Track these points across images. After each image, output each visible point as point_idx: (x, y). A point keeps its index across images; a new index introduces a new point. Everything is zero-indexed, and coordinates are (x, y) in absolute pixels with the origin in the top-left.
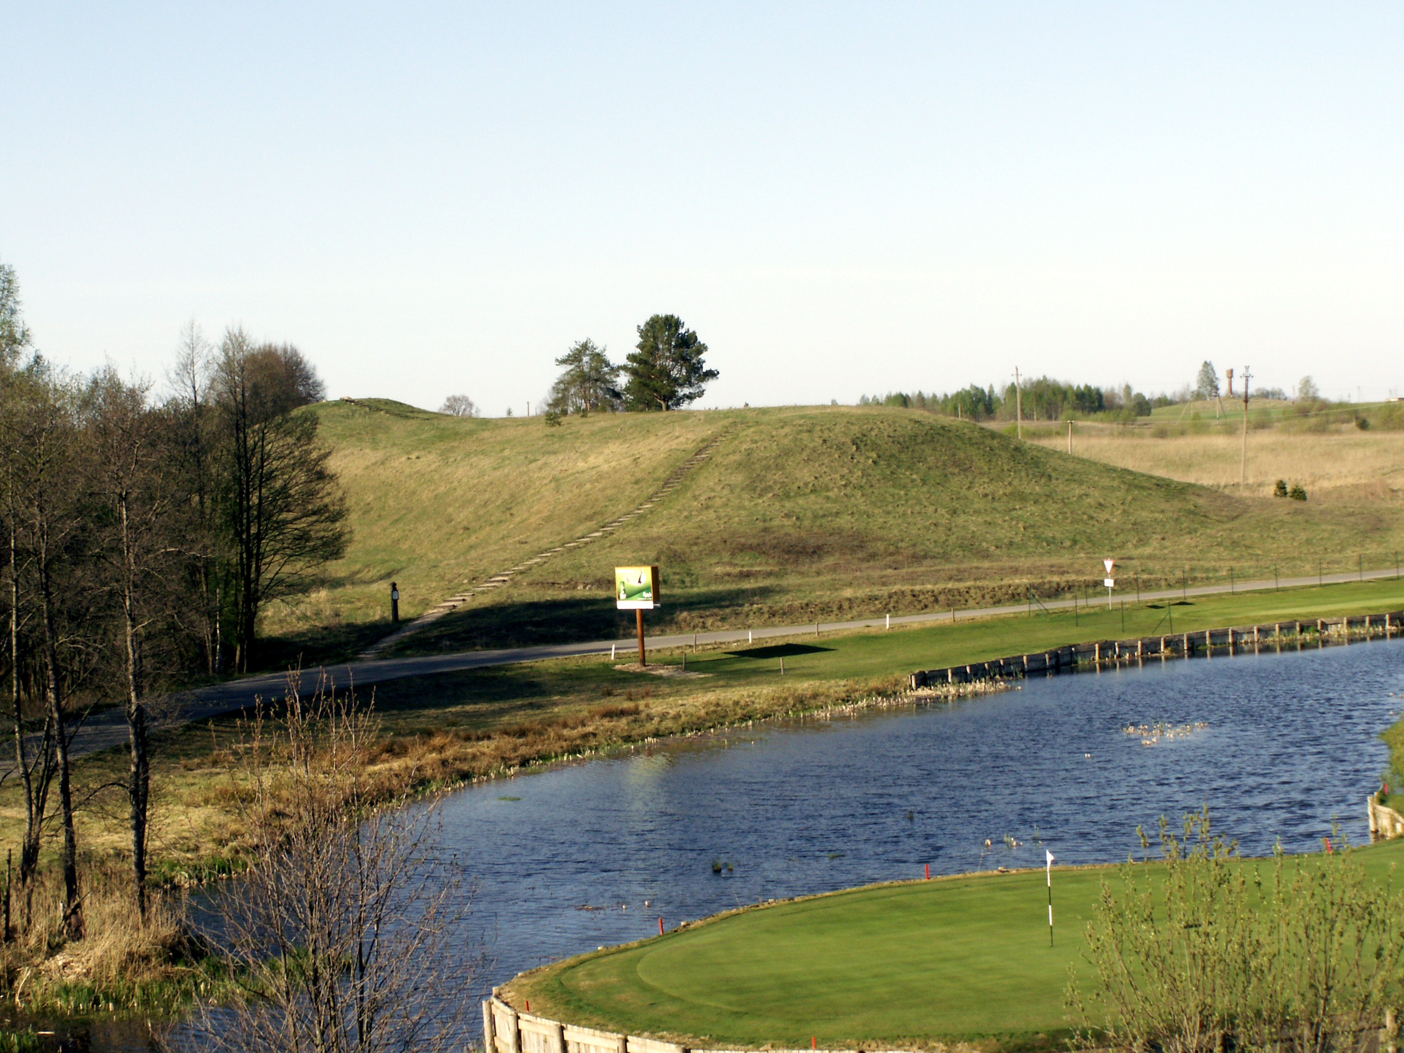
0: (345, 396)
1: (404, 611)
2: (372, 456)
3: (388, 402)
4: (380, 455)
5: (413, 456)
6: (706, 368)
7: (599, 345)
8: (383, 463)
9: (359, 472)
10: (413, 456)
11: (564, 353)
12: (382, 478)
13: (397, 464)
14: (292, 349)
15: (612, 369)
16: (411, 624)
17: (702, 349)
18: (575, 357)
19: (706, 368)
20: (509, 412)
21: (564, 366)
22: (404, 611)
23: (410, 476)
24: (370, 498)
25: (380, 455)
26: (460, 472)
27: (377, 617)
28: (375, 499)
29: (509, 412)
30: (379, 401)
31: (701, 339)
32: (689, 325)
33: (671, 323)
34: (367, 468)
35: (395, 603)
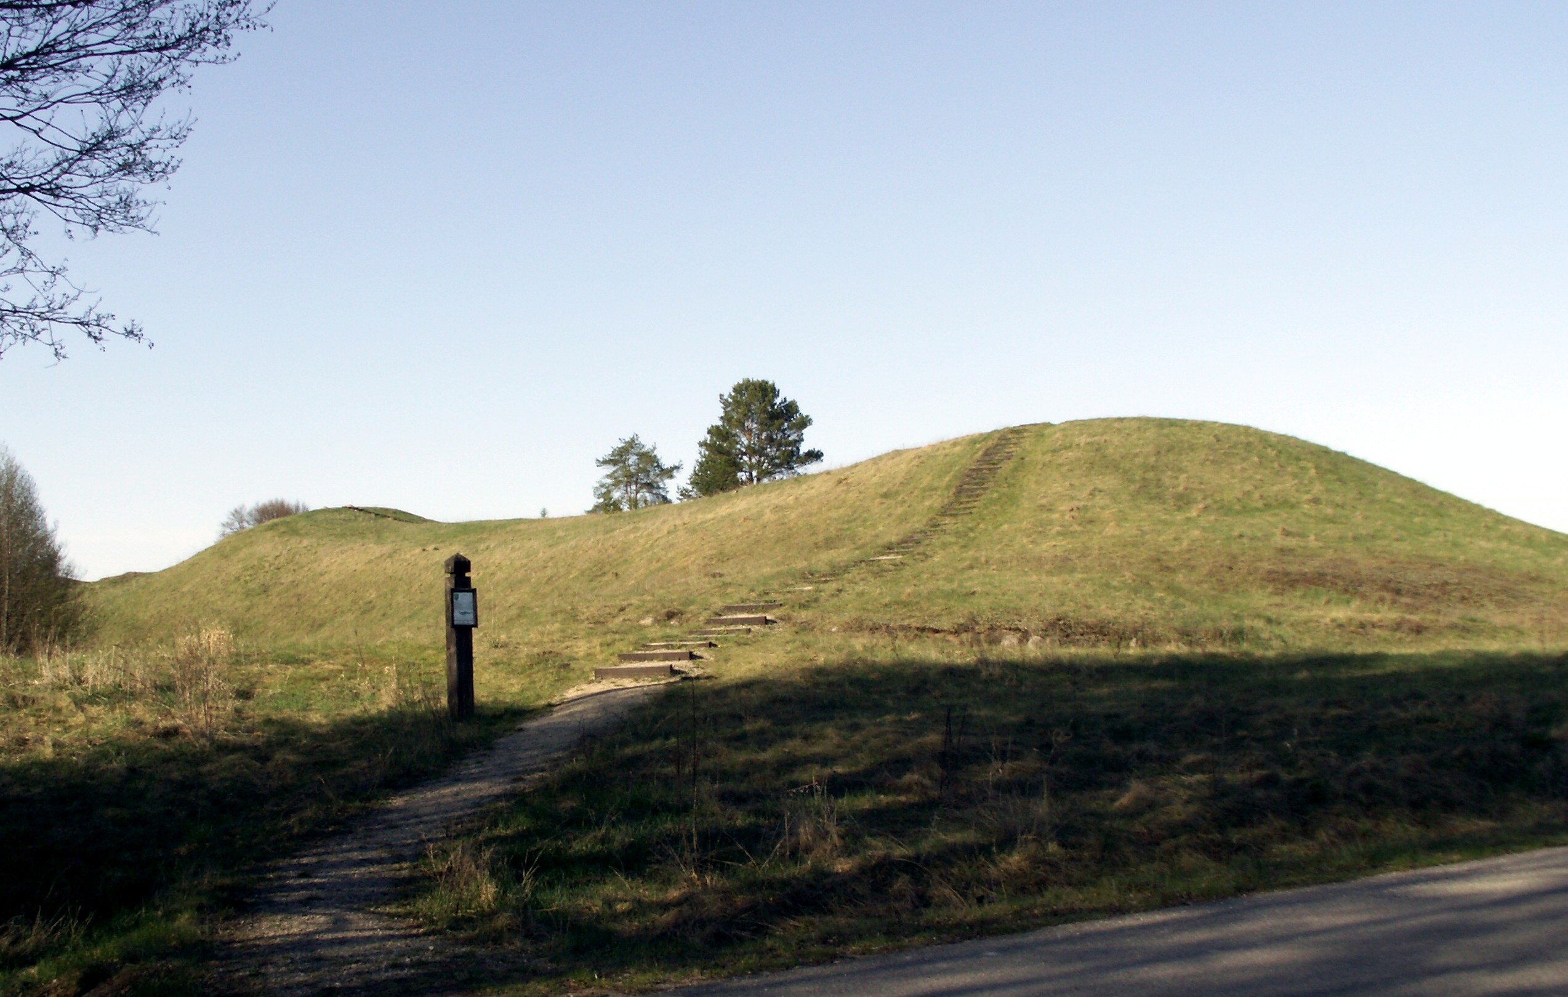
0: (348, 504)
1: (491, 684)
2: (375, 550)
3: (396, 512)
4: (387, 548)
5: (430, 548)
6: (804, 448)
7: (647, 442)
8: (390, 556)
9: (359, 567)
10: (430, 548)
11: (606, 452)
12: (390, 572)
13: (408, 556)
14: (304, 507)
15: (662, 470)
16: (532, 725)
17: (805, 422)
18: (618, 458)
19: (804, 448)
20: (544, 514)
21: (608, 466)
22: (491, 684)
23: (427, 568)
24: (372, 595)
25: (387, 548)
26: (497, 556)
27: (386, 701)
28: (379, 596)
29: (544, 514)
30: (387, 510)
31: (804, 410)
32: (786, 393)
33: (766, 390)
34: (370, 562)
35: (461, 637)
